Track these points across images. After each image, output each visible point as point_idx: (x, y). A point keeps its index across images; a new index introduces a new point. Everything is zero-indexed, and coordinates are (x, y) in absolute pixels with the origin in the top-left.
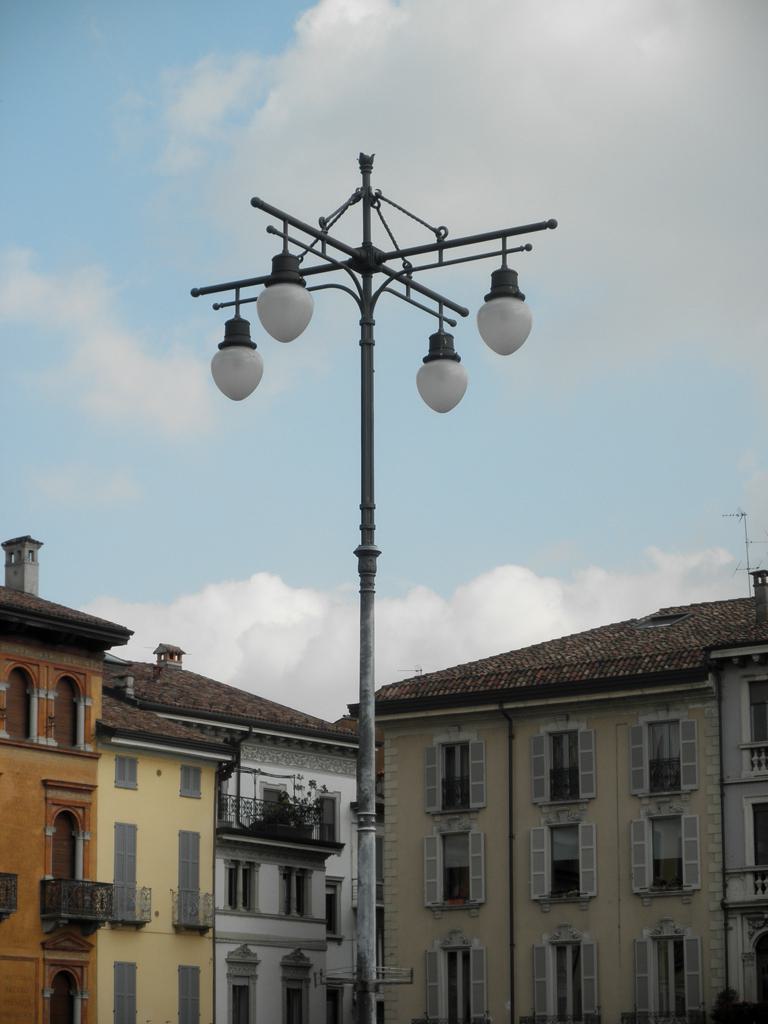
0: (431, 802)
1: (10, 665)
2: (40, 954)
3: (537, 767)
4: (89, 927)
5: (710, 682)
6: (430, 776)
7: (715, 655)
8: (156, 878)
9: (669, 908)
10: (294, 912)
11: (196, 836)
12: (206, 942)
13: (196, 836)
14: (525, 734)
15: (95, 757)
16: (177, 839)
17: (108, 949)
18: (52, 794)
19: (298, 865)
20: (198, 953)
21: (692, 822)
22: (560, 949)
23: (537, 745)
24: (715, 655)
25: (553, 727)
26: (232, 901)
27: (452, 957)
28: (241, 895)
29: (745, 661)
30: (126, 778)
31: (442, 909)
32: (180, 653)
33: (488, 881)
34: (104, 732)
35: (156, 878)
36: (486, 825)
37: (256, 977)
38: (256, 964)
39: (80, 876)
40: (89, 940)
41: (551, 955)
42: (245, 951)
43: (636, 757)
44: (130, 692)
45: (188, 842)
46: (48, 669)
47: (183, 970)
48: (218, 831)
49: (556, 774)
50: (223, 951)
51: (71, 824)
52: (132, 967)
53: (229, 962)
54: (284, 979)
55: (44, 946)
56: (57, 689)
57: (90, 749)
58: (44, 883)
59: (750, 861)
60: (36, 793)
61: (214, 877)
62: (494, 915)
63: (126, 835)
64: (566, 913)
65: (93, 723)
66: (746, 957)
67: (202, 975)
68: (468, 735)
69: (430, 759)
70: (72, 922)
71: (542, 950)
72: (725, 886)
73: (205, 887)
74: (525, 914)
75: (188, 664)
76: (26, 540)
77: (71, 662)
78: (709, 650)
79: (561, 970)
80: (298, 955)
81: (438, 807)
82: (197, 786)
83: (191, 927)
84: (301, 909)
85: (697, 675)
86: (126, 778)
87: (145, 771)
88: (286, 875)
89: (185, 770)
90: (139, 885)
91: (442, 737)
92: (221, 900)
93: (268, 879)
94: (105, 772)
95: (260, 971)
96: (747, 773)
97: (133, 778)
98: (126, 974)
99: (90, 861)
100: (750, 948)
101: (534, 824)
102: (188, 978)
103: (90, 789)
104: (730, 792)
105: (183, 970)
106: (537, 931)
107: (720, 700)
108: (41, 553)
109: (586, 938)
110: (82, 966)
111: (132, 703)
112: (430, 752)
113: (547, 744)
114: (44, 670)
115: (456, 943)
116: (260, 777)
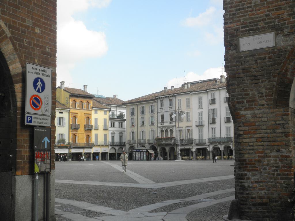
0: (150, 112)
1: (80, 101)
2: (84, 133)
3: (140, 110)
4: (91, 130)
5: (156, 100)
6: (130, 111)
7: (156, 97)
8: (101, 124)
9: (153, 127)
10: (121, 127)
11: (106, 119)
12: (108, 131)
13: (106, 119)
14: (139, 107)
15: (92, 110)
16: (103, 120)
17: (94, 132)
18: (85, 115)
19: (121, 122)
20: (106, 132)
21: (155, 117)
22: (152, 131)
23: (140, 108)
24: (156, 97)
25: (131, 107)
26: (111, 126)
27: (143, 132)
28: (113, 125)
29: (159, 98)
30: (96, 113)
31: (131, 127)
32: (116, 96)
33: (135, 124)
34: (92, 107)
35: (101, 124)
36: (135, 117)
37: (123, 135)
38: (123, 134)
39: (90, 124)
40: (91, 131)
41: (141, 132)
42: (113, 132)
43: (149, 110)
44: (101, 102)
45: (105, 120)
46: (85, 101)
47: (104, 134)
48: (109, 118)
49: (132, 113)
50: (110, 132)
51: (88, 118)
52: (97, 134)
53: (111, 133)
54: (119, 135)
55: (85, 132)
56: (86, 103)
57: (91, 109)
58: (85, 125)
59: (160, 121)
60: (84, 115)
61: (109, 123)
62: (136, 127)
63: (96, 120)
64: (143, 127)
65: (91, 106)
66: (160, 132)
67: (107, 135)
68: (134, 107)
69: (130, 110)
70: (88, 129)
71: (130, 132)
72: (158, 124)
73: (107, 125)
74: (139, 128)
75: (117, 97)
76: (86, 85)
77: (88, 100)
78: (156, 97)
79: (143, 134)
80: (121, 132)
81: (131, 115)
82: (106, 113)
83: (105, 129)
84: (122, 127)
85: (155, 100)
86: (96, 113)
87: (99, 112)
88: (119, 123)
89: (104, 111)
90: (98, 125)
91: (131, 107)
92: (110, 126)
93: (117, 124)
94: (93, 112)
95: (115, 134)
96: (160, 111)
97: (97, 112)
98: (96, 135)
99: (91, 122)
100: (160, 131)
101: (140, 117)
102: (105, 136)
103: (91, 114)
104: (158, 113)
105: (104, 134)
106: (140, 130)
107: (157, 102)
108: (87, 87)
109: (145, 130)
110: (90, 134)
111: (101, 103)
112: (130, 109)
113: (131, 109)
114: (77, 100)
115: (143, 130)
116: (118, 112)
